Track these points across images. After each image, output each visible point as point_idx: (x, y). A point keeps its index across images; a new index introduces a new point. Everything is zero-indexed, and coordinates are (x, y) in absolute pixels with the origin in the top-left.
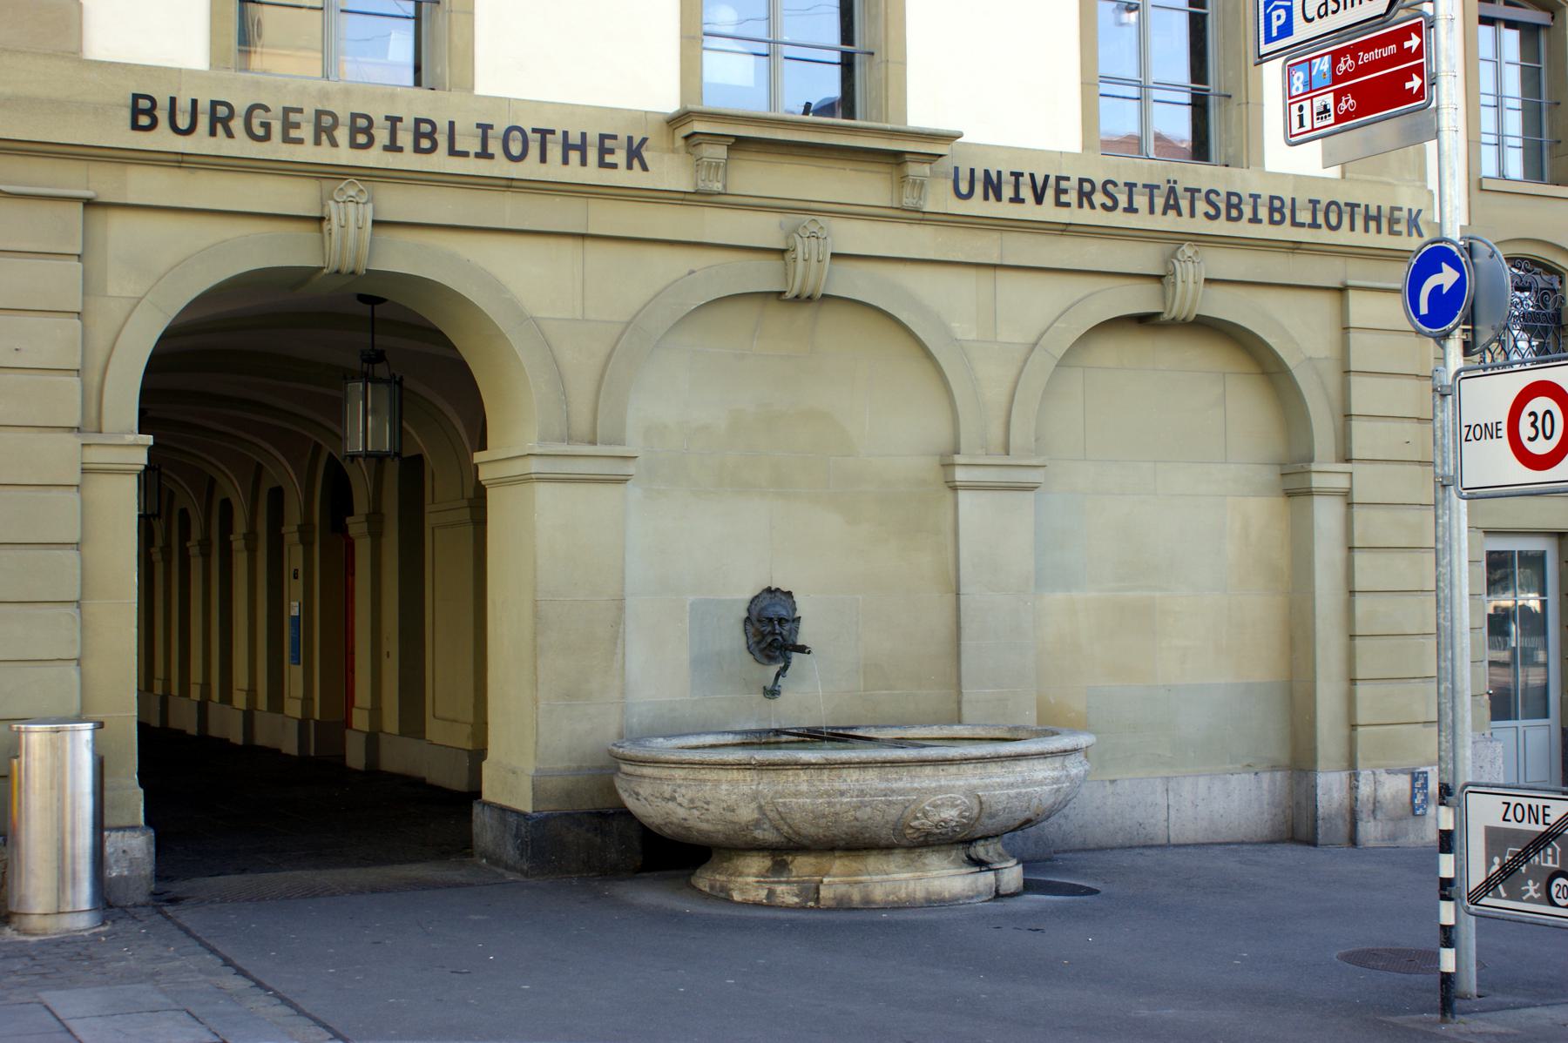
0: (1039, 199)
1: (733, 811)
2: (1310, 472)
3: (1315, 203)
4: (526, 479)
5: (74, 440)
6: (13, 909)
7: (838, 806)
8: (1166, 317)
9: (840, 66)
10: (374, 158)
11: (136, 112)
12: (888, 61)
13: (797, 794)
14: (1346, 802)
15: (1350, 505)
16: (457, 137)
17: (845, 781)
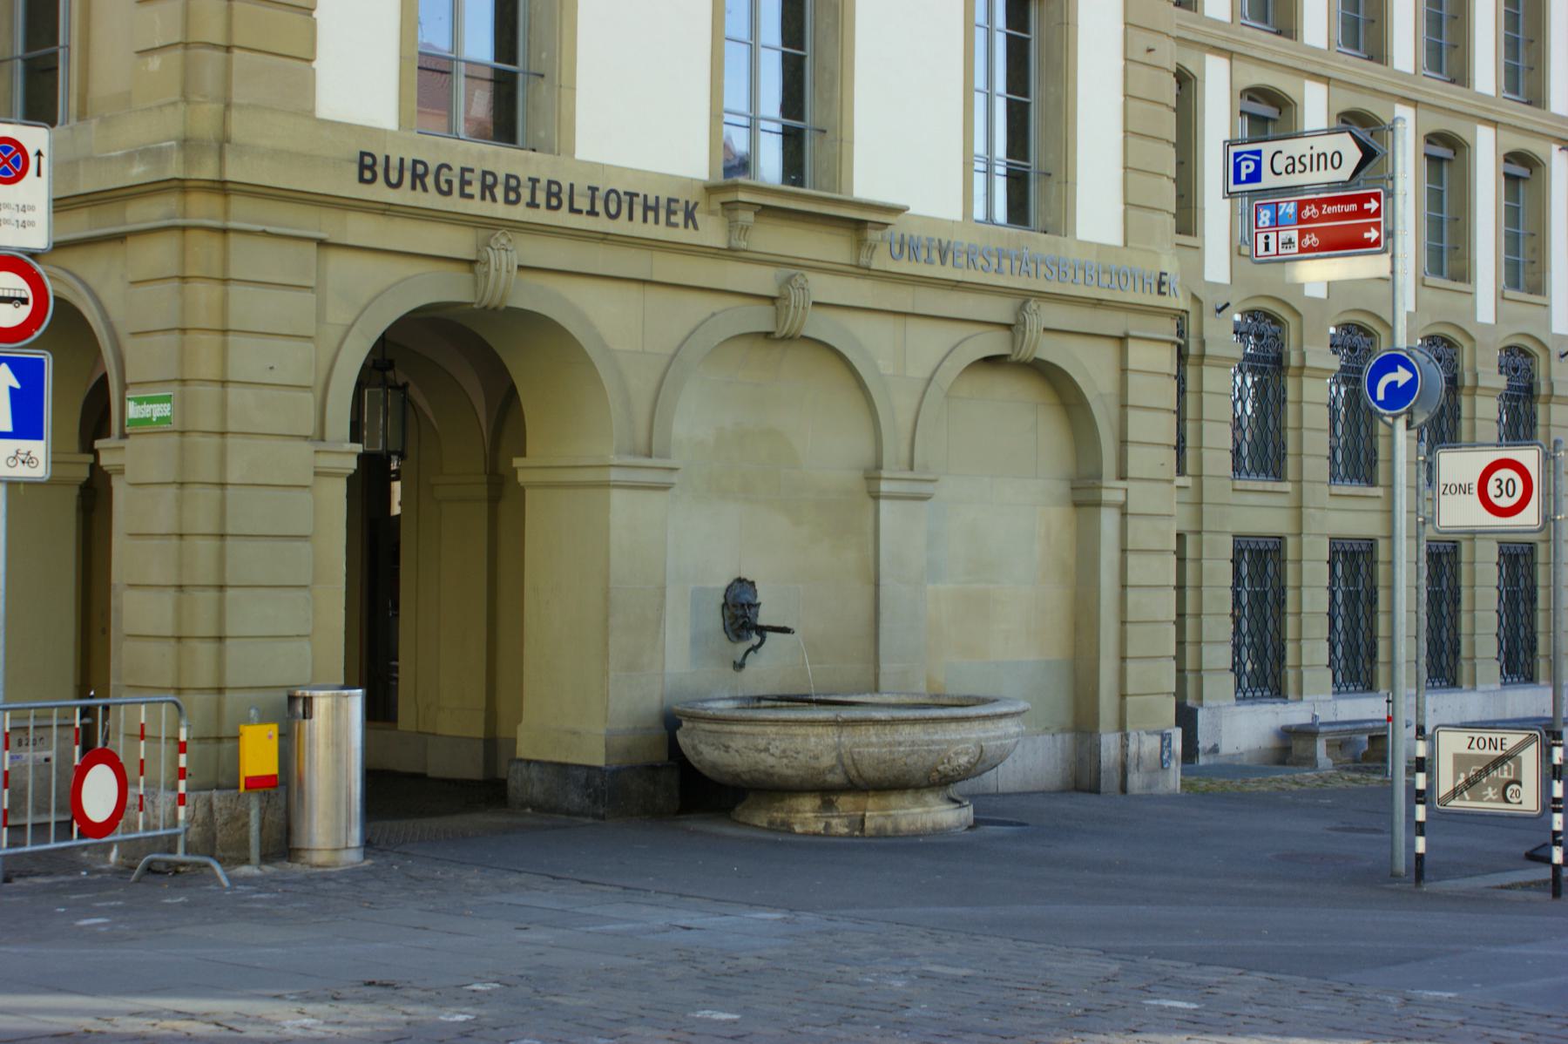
0: (943, 263)
1: (818, 758)
2: (879, 478)
3: (593, 190)
4: (606, 485)
5: (307, 448)
6: (296, 846)
7: (896, 754)
8: (1014, 358)
9: (781, 136)
10: (520, 213)
11: (362, 167)
12: (561, 86)
13: (870, 744)
14: (1119, 758)
15: (1124, 515)
16: (575, 197)
17: (901, 734)
